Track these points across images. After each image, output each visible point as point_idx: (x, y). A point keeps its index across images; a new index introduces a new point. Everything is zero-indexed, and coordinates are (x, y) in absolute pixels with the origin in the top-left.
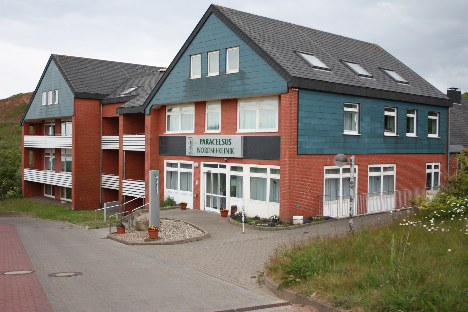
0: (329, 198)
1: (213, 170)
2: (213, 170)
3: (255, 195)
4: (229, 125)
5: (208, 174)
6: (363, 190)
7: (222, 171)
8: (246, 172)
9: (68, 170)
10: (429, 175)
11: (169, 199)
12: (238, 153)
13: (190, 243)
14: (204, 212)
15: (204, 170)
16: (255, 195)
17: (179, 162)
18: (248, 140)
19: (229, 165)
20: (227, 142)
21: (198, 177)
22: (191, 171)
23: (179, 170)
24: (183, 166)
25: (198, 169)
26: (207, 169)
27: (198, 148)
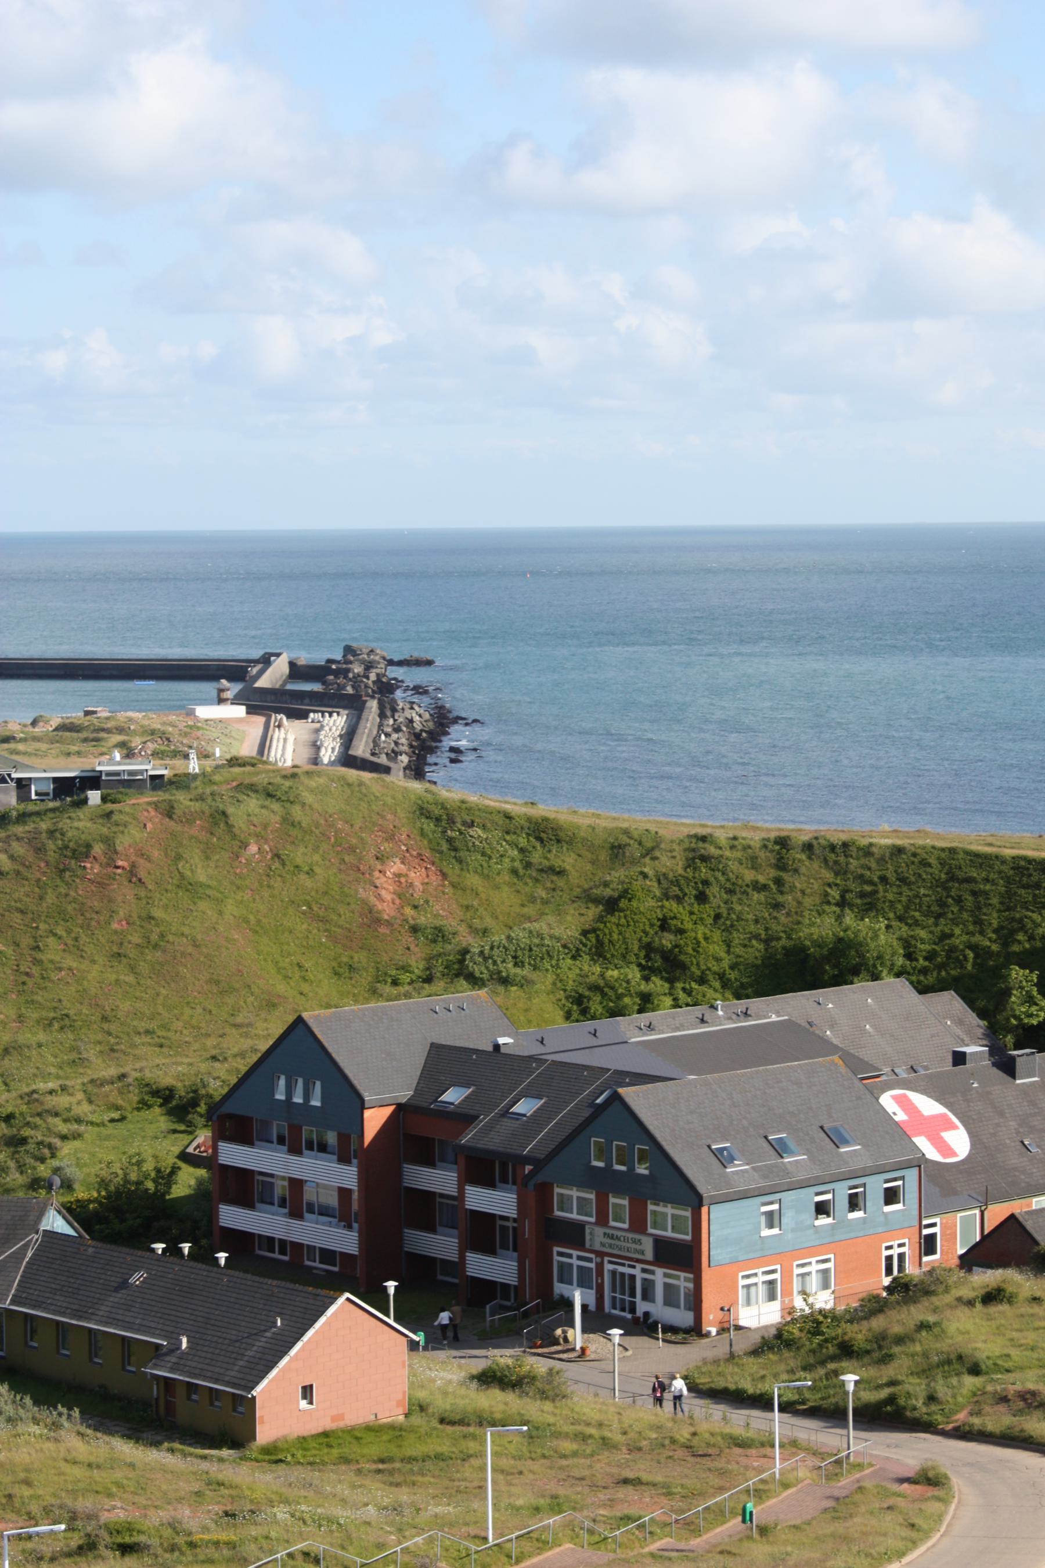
1: (621, 1269)
2: (621, 1269)
8: (660, 1276)
12: (649, 1256)
15: (608, 1267)
17: (575, 1253)
18: (660, 1244)
19: (639, 1266)
22: (592, 1265)
23: (575, 1262)
24: (579, 1258)
25: (600, 1267)
26: (611, 1267)
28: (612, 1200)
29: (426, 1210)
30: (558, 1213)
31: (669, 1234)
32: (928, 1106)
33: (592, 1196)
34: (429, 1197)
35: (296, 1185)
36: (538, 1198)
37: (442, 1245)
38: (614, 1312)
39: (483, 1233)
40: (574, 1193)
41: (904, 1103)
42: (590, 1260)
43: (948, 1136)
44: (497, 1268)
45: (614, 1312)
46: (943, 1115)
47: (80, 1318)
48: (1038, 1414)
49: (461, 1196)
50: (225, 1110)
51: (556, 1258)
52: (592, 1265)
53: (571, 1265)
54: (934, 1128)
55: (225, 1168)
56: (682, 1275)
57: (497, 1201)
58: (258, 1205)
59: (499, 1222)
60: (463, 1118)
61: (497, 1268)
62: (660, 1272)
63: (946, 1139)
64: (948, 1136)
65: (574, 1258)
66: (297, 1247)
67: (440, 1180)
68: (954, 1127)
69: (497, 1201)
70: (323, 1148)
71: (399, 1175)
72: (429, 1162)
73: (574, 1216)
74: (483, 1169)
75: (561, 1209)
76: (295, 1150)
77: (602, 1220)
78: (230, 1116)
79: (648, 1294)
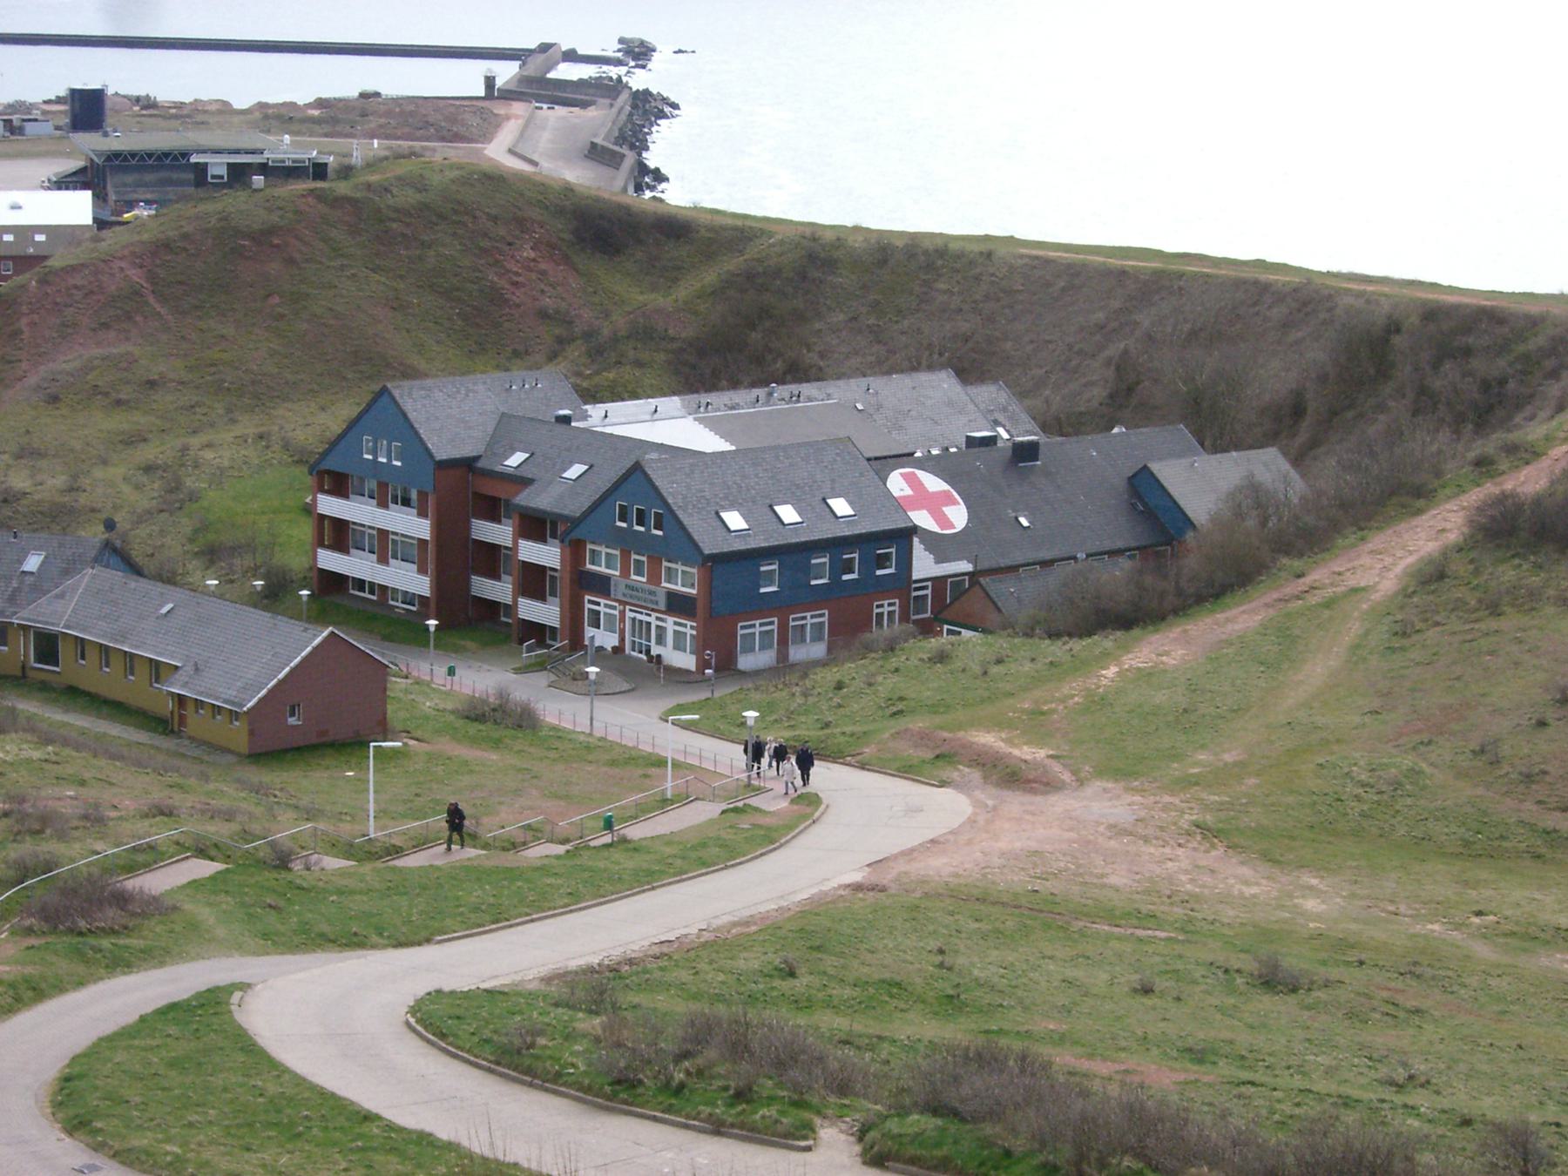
0: (744, 651)
1: (639, 617)
2: (639, 617)
3: (677, 647)
4: (655, 578)
5: (634, 619)
6: (783, 642)
7: (647, 619)
8: (670, 623)
9: (372, 552)
10: (880, 615)
11: (795, 1136)
12: (662, 606)
13: (302, 744)
14: (630, 657)
15: (629, 615)
16: (677, 647)
17: (602, 601)
18: (671, 595)
19: (654, 615)
20: (652, 593)
21: (622, 619)
22: (616, 613)
23: (601, 609)
24: (606, 606)
25: (623, 613)
26: (633, 615)
27: (675, 106)
28: (634, 557)
29: (491, 559)
30: (589, 566)
31: (679, 588)
32: (934, 483)
33: (617, 553)
34: (494, 548)
35: (383, 534)
36: (575, 550)
37: (499, 590)
38: (635, 654)
39: (534, 581)
40: (603, 550)
41: (911, 480)
42: (614, 608)
43: (949, 511)
44: (546, 612)
45: (635, 654)
46: (946, 493)
47: (116, 641)
48: (6, 977)
49: (514, 549)
50: (326, 465)
51: (588, 606)
52: (616, 613)
53: (598, 613)
54: (934, 504)
55: (322, 517)
56: (689, 624)
57: (546, 554)
58: (353, 551)
59: (549, 573)
60: (520, 481)
61: (546, 612)
62: (671, 620)
63: (408, 406)
64: (949, 511)
65: (604, 607)
66: (384, 589)
67: (498, 533)
68: (955, 503)
69: (546, 554)
70: (406, 502)
71: (468, 528)
72: (495, 518)
73: (602, 569)
74: (536, 526)
75: (593, 563)
76: (383, 504)
77: (625, 573)
78: (328, 472)
79: (661, 640)
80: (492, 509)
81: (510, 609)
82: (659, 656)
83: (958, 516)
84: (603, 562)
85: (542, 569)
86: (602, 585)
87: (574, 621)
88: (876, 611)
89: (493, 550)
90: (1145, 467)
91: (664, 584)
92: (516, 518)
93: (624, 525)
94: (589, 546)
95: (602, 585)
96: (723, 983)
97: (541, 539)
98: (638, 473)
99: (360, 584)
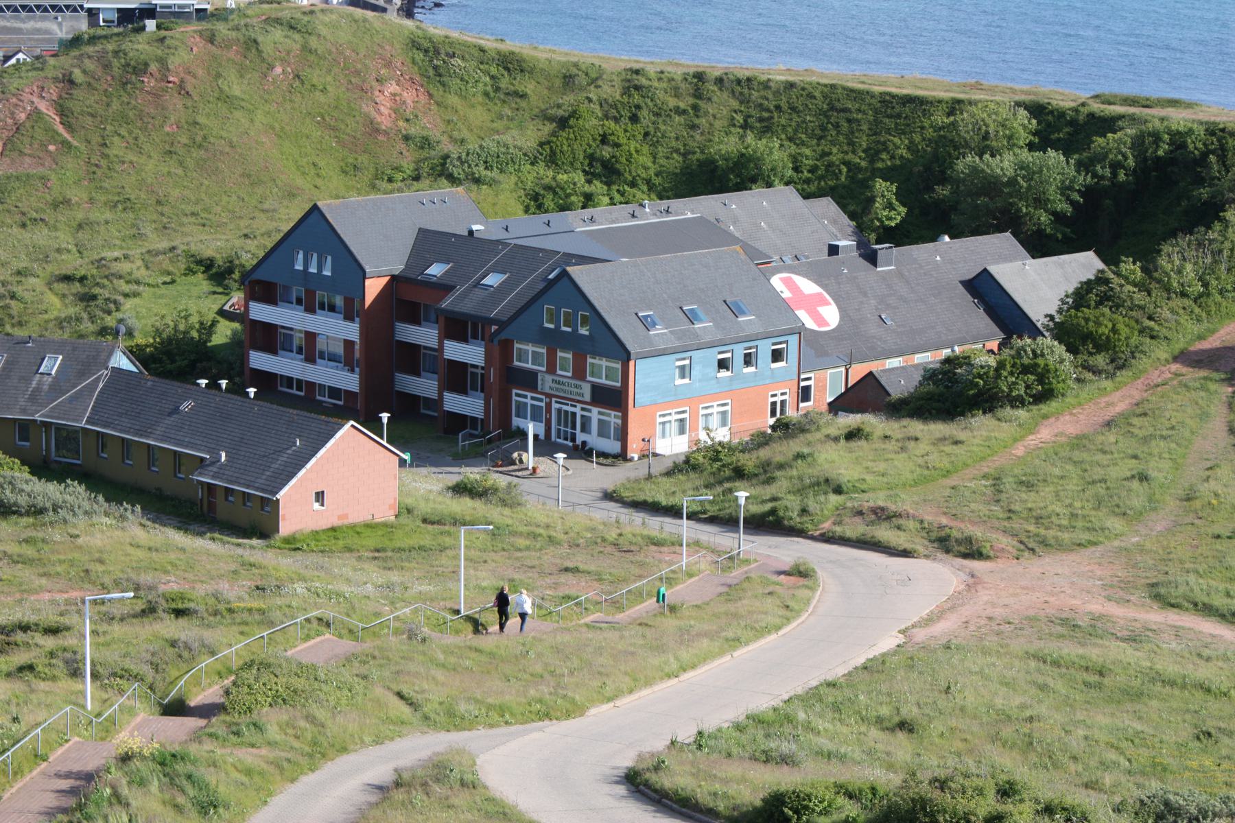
1: (565, 408)
2: (565, 408)
5: (559, 410)
7: (573, 409)
8: (595, 413)
12: (587, 398)
15: (555, 406)
17: (529, 394)
19: (579, 406)
22: (543, 404)
23: (529, 401)
24: (532, 398)
25: (549, 406)
26: (558, 406)
28: (560, 354)
29: (412, 359)
30: (516, 363)
31: (603, 381)
32: (808, 287)
33: (544, 351)
35: (311, 337)
37: (425, 386)
39: (458, 377)
40: (530, 348)
42: (541, 400)
44: (469, 405)
46: (819, 294)
47: (141, 436)
49: (441, 348)
51: (514, 398)
52: (543, 404)
54: (812, 304)
55: (255, 323)
56: (613, 413)
57: (470, 353)
59: (470, 369)
60: (443, 287)
61: (469, 405)
62: (595, 410)
65: (529, 399)
66: (311, 386)
67: (425, 335)
68: (828, 304)
69: (470, 353)
70: (332, 308)
72: (416, 321)
74: (458, 327)
76: (310, 309)
77: (551, 369)
78: (258, 282)
79: (585, 428)
80: (414, 315)
81: (437, 403)
82: (584, 443)
83: (831, 315)
84: (528, 355)
85: (464, 366)
86: (529, 380)
87: (503, 410)
88: (659, 420)
89: (414, 349)
90: (985, 270)
91: (589, 378)
92: (442, 320)
93: (569, 329)
94: (516, 346)
95: (529, 380)
96: (1178, 394)
97: (463, 339)
98: (565, 279)
99: (289, 381)
